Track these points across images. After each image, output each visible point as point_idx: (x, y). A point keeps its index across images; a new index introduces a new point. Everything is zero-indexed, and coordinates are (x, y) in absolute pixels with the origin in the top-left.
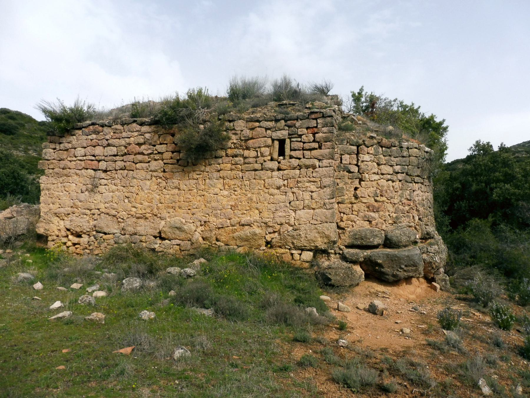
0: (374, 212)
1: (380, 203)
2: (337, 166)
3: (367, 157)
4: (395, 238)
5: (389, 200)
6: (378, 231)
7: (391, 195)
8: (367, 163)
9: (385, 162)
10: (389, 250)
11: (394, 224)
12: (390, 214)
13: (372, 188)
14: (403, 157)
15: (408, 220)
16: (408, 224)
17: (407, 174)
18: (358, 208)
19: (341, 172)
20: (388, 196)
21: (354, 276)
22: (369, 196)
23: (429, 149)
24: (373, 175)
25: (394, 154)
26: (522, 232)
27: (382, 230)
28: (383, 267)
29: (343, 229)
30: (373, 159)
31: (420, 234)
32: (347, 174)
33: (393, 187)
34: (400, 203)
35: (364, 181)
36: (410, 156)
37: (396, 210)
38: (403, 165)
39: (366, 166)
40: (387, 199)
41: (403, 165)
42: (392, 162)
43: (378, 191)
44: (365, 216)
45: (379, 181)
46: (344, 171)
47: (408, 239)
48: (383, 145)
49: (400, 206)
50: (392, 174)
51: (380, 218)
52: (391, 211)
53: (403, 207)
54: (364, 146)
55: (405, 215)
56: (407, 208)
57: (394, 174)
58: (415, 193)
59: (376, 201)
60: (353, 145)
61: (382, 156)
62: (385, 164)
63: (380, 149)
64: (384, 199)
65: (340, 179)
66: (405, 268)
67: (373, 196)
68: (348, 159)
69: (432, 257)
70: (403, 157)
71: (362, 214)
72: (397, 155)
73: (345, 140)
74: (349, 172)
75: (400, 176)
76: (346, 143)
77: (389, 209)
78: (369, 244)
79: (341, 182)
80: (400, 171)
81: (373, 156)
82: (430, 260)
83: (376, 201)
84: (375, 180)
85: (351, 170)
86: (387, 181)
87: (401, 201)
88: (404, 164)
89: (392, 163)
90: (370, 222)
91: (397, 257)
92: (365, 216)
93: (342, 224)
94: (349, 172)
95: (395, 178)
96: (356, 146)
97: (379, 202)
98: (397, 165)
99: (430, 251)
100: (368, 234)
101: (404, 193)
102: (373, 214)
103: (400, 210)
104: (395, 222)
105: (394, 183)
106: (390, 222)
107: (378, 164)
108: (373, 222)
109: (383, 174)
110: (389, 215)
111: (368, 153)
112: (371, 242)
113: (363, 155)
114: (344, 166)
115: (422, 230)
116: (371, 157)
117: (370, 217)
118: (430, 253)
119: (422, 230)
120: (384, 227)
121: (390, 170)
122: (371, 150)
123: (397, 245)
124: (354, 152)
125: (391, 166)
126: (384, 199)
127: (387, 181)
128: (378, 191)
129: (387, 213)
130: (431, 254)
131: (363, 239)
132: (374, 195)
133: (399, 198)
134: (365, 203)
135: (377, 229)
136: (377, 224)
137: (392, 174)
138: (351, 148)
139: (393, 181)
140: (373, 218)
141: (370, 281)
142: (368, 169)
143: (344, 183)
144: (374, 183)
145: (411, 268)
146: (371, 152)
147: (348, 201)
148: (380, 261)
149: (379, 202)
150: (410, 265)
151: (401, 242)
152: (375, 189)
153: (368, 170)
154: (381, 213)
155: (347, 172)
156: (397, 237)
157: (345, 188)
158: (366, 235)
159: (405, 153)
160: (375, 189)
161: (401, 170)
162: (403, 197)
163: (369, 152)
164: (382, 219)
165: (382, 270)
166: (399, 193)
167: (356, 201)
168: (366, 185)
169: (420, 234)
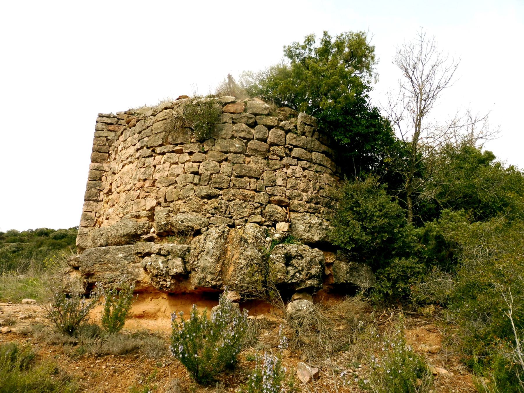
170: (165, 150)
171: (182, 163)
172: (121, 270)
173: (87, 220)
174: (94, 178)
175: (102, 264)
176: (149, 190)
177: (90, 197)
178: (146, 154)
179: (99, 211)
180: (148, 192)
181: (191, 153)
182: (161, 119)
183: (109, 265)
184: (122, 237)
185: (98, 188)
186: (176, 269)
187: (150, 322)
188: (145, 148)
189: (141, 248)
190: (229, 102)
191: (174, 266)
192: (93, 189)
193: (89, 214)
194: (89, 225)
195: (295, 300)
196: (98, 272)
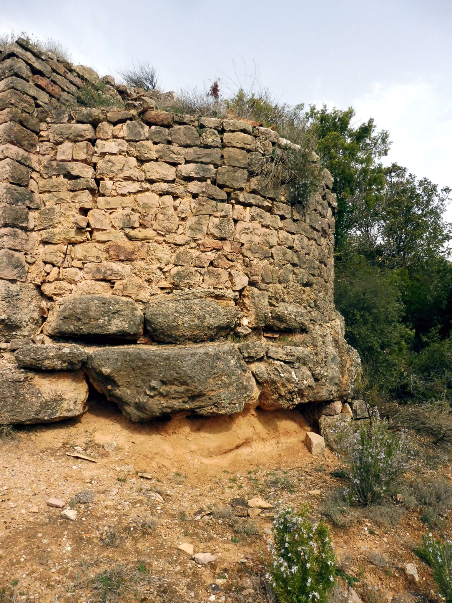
0: (122, 261)
1: (139, 243)
2: (45, 167)
3: (111, 146)
4: (160, 319)
5: (163, 236)
6: (127, 303)
7: (166, 224)
8: (112, 158)
9: (154, 156)
10: (153, 348)
11: (175, 291)
12: (162, 266)
13: (121, 211)
14: (207, 147)
15: (212, 281)
16: (212, 290)
17: (214, 182)
18: (85, 253)
19: (54, 177)
20: (160, 228)
21: (24, 400)
22: (113, 226)
23: (289, 142)
24: (124, 183)
25: (179, 139)
26: (311, 206)
27: (137, 301)
28: (114, 383)
29: (50, 299)
30: (125, 149)
31: (252, 318)
32: (66, 180)
33: (176, 209)
34: (193, 245)
35: (103, 195)
36: (224, 146)
37: (178, 257)
38: (202, 163)
39: (110, 164)
40: (159, 234)
41: (202, 163)
42: (174, 156)
43: (135, 217)
44: (98, 270)
45: (139, 195)
46: (58, 176)
47: (197, 322)
48: (152, 120)
49: (192, 251)
50: (173, 181)
51: (137, 275)
52: (164, 261)
53: (198, 253)
54: (105, 123)
55: (203, 271)
56: (211, 256)
57: (177, 180)
58: (240, 226)
59: (130, 238)
60: (82, 122)
61: (149, 143)
62: (156, 160)
63: (147, 128)
64: (149, 233)
65: (50, 192)
66: (163, 389)
67: (122, 225)
68: (70, 151)
69: (276, 369)
70: (207, 147)
71: (90, 265)
72: (189, 142)
73: (64, 113)
74: (69, 176)
75: (194, 187)
76: (67, 119)
77: (160, 255)
78: (97, 331)
79: (50, 199)
80: (193, 175)
81: (126, 144)
82: (273, 376)
83: (130, 238)
84: (130, 193)
85: (74, 173)
86: (161, 195)
87: (195, 240)
88: (207, 160)
89: (173, 159)
90: (112, 283)
91: (140, 359)
92: (98, 270)
93: (48, 289)
94: (69, 176)
95: (179, 189)
96: (90, 123)
97: (137, 239)
98: (187, 162)
99: (274, 356)
100: (93, 309)
101: (204, 221)
102: (116, 266)
103: (192, 258)
104: (176, 286)
105: (178, 201)
106: (165, 284)
107: (141, 161)
108: (117, 285)
109: (151, 181)
110: (161, 269)
111: (115, 137)
112: (100, 327)
113: (104, 142)
114: (58, 165)
115: (256, 306)
116: (119, 145)
117: (109, 272)
118: (274, 359)
119: (256, 306)
120: (145, 295)
121: (170, 173)
122: (123, 130)
123: (170, 336)
124: (82, 136)
125: (175, 164)
126: (149, 233)
127: (161, 195)
128: (135, 217)
129: (156, 265)
130: (276, 362)
131: (79, 319)
132: (124, 223)
133: (189, 232)
134: (104, 242)
135: (125, 299)
136: (125, 288)
137: (173, 181)
138: (76, 128)
139: (176, 197)
140: (114, 273)
141: (118, 422)
142: (112, 169)
143: (56, 199)
144: (128, 200)
145: (174, 388)
146: (121, 134)
147: (62, 237)
148: (106, 370)
149: (137, 239)
150: (171, 379)
151: (176, 328)
152: (128, 211)
153: (112, 172)
154: (139, 264)
155: (65, 176)
156: (167, 316)
157: (57, 210)
158: (88, 309)
159: (211, 139)
160: (128, 211)
161: (196, 173)
162: (200, 230)
163: (116, 133)
164: (141, 277)
165: (118, 392)
166: (188, 223)
167: (79, 238)
168: (108, 203)
169: (254, 316)
170: (253, 201)
171: (276, 230)
172: (235, 384)
173: (16, 268)
174: (19, 179)
175: (215, 378)
176: (233, 258)
177: (16, 219)
178: (218, 195)
179: (32, 251)
180: (232, 261)
181: (283, 218)
182: (239, 145)
183: (223, 378)
184: (211, 329)
185: (27, 203)
186: (306, 380)
187: (245, 450)
188: (209, 181)
189: (253, 350)
190: (58, 71)
191: (305, 377)
192: (20, 204)
193: (17, 254)
194: (18, 279)
195: (366, 405)
196: (213, 390)
